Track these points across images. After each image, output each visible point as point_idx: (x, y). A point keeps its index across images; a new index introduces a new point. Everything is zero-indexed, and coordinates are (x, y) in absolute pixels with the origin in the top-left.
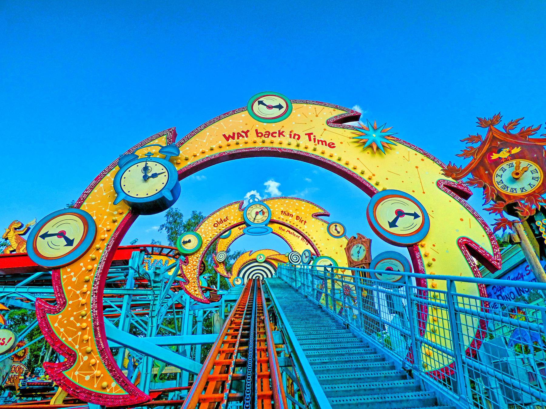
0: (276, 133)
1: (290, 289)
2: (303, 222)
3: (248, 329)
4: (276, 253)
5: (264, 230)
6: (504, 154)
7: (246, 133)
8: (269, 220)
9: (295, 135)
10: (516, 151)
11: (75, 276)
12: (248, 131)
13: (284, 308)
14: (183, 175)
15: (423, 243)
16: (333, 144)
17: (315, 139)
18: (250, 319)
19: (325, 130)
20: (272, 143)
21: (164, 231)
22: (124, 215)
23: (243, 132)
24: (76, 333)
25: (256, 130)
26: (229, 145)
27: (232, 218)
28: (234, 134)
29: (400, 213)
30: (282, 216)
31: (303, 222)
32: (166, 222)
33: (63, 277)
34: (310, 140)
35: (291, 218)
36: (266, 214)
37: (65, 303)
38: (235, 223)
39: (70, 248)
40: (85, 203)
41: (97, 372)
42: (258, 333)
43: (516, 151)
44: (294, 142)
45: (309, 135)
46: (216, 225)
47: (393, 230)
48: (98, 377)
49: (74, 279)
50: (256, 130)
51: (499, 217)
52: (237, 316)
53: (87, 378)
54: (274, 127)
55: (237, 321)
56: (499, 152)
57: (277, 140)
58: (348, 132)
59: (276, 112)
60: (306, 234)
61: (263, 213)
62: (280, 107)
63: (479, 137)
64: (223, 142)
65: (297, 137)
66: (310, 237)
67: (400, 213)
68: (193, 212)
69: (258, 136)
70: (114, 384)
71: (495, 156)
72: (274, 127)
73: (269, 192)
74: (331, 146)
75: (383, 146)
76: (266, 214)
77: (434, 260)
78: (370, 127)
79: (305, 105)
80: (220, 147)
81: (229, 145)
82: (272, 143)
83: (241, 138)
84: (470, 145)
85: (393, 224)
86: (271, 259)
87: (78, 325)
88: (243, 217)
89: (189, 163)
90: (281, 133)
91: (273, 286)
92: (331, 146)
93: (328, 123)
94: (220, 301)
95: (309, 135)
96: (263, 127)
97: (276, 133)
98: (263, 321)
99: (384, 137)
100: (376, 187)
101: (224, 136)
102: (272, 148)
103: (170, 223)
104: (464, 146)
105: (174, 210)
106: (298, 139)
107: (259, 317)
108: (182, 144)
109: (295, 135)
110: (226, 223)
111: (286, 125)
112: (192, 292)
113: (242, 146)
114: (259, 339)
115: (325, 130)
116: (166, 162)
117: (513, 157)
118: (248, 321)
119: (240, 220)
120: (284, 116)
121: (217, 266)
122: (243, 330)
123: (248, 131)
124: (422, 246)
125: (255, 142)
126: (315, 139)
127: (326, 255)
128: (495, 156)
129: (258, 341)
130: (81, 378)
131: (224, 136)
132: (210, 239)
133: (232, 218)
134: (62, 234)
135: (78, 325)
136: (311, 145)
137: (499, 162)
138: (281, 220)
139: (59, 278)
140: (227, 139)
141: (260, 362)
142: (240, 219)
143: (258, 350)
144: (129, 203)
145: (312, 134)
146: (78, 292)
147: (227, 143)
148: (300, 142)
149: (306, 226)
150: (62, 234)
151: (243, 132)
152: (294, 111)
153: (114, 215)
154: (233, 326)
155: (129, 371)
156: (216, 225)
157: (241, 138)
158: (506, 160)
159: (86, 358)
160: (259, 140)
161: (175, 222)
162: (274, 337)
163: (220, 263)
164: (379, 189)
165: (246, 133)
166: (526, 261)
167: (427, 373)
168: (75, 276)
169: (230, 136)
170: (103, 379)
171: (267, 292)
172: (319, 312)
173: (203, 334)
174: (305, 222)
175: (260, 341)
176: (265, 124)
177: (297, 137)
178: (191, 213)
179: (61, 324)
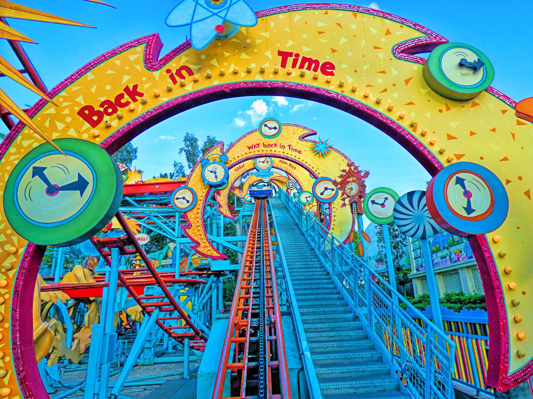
0: (273, 145)
1: (284, 210)
2: (294, 168)
3: (260, 235)
4: (279, 175)
5: (268, 174)
6: (351, 179)
7: (258, 145)
8: (271, 166)
9: (282, 146)
10: (354, 179)
11: (193, 215)
12: (259, 144)
13: (278, 224)
14: (230, 168)
15: (334, 202)
16: (301, 151)
17: (292, 148)
18: (261, 230)
19: (298, 143)
20: (271, 151)
21: (184, 154)
22: (207, 189)
23: (257, 144)
24: (198, 236)
25: (263, 143)
26: (250, 152)
27: (247, 165)
28: (252, 145)
29: (326, 189)
30: (280, 164)
31: (294, 168)
32: (184, 146)
33: (188, 215)
34: (290, 149)
35: (286, 165)
36: (269, 163)
37: (192, 225)
38: (249, 168)
39: (188, 204)
40: (189, 183)
41: (208, 249)
42: (266, 272)
43: (354, 179)
44: (281, 150)
45: (289, 146)
46: (236, 170)
47: (322, 196)
48: (209, 250)
49: (193, 216)
50: (263, 143)
51: (343, 202)
52: (253, 228)
53: (206, 251)
54: (272, 141)
55: (254, 230)
56: (349, 178)
57: (274, 149)
58: (309, 144)
59: (274, 132)
60: (296, 177)
61: (268, 162)
62: (275, 128)
63: (346, 170)
64: (247, 151)
65: (283, 147)
66: (297, 179)
67: (326, 189)
68: (208, 137)
69: (264, 147)
70: (215, 252)
71: (348, 180)
72: (272, 141)
73: (275, 101)
74: (300, 152)
75: (325, 153)
76: (269, 163)
77: (337, 209)
78: (320, 142)
79: (289, 127)
80: (246, 154)
81: (250, 152)
82: (271, 151)
83: (256, 148)
84: (342, 173)
85: (322, 194)
86: (276, 180)
87: (198, 233)
88: (254, 165)
89: (232, 163)
90: (275, 145)
91: (274, 207)
92: (300, 152)
93: (299, 138)
94: (239, 216)
95: (289, 146)
96: (267, 141)
97: (273, 145)
98: (267, 231)
99: (326, 148)
100: (318, 175)
101: (248, 147)
102: (271, 154)
103: (188, 146)
104: (341, 173)
105: (190, 135)
106: (284, 148)
107: (265, 229)
108: (228, 152)
109: (282, 146)
110: (243, 168)
111: (278, 140)
112: (224, 212)
113: (257, 153)
114: (268, 306)
115: (298, 143)
116: (222, 164)
117: (353, 181)
118: (259, 231)
119: (252, 166)
120: (278, 134)
121: (235, 190)
122: (258, 235)
123: (259, 144)
124: (333, 203)
125: (263, 151)
126: (292, 148)
127: (307, 190)
128: (348, 180)
129: (266, 287)
130: (204, 251)
131: (248, 147)
132: (233, 179)
133: (247, 165)
134: (184, 198)
135: (198, 233)
136: (290, 152)
137: (348, 182)
138: (279, 167)
139: (187, 216)
140: (249, 149)
141: (266, 266)
142: (252, 166)
143: (266, 287)
144: (209, 184)
145: (291, 145)
146: (196, 221)
147: (249, 151)
148: (285, 150)
149: (295, 171)
150: (184, 198)
151: (257, 144)
152: (282, 131)
153: (203, 189)
154: (253, 233)
155: (173, 260)
156: (236, 170)
157: (256, 148)
158: (351, 182)
159: (204, 244)
160: (264, 149)
161: (192, 145)
162: (271, 238)
163: (236, 188)
164: (319, 176)
165: (258, 145)
166: (41, 289)
167: (406, 270)
168: (193, 215)
169: (250, 147)
170: (212, 251)
171: (270, 210)
172: (295, 227)
173: (181, 238)
174: (295, 168)
175: (266, 251)
176: (268, 139)
177: (283, 147)
178: (206, 138)
179: (192, 233)
